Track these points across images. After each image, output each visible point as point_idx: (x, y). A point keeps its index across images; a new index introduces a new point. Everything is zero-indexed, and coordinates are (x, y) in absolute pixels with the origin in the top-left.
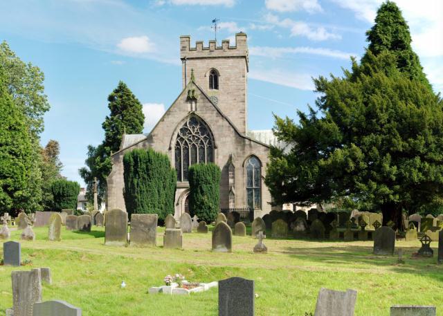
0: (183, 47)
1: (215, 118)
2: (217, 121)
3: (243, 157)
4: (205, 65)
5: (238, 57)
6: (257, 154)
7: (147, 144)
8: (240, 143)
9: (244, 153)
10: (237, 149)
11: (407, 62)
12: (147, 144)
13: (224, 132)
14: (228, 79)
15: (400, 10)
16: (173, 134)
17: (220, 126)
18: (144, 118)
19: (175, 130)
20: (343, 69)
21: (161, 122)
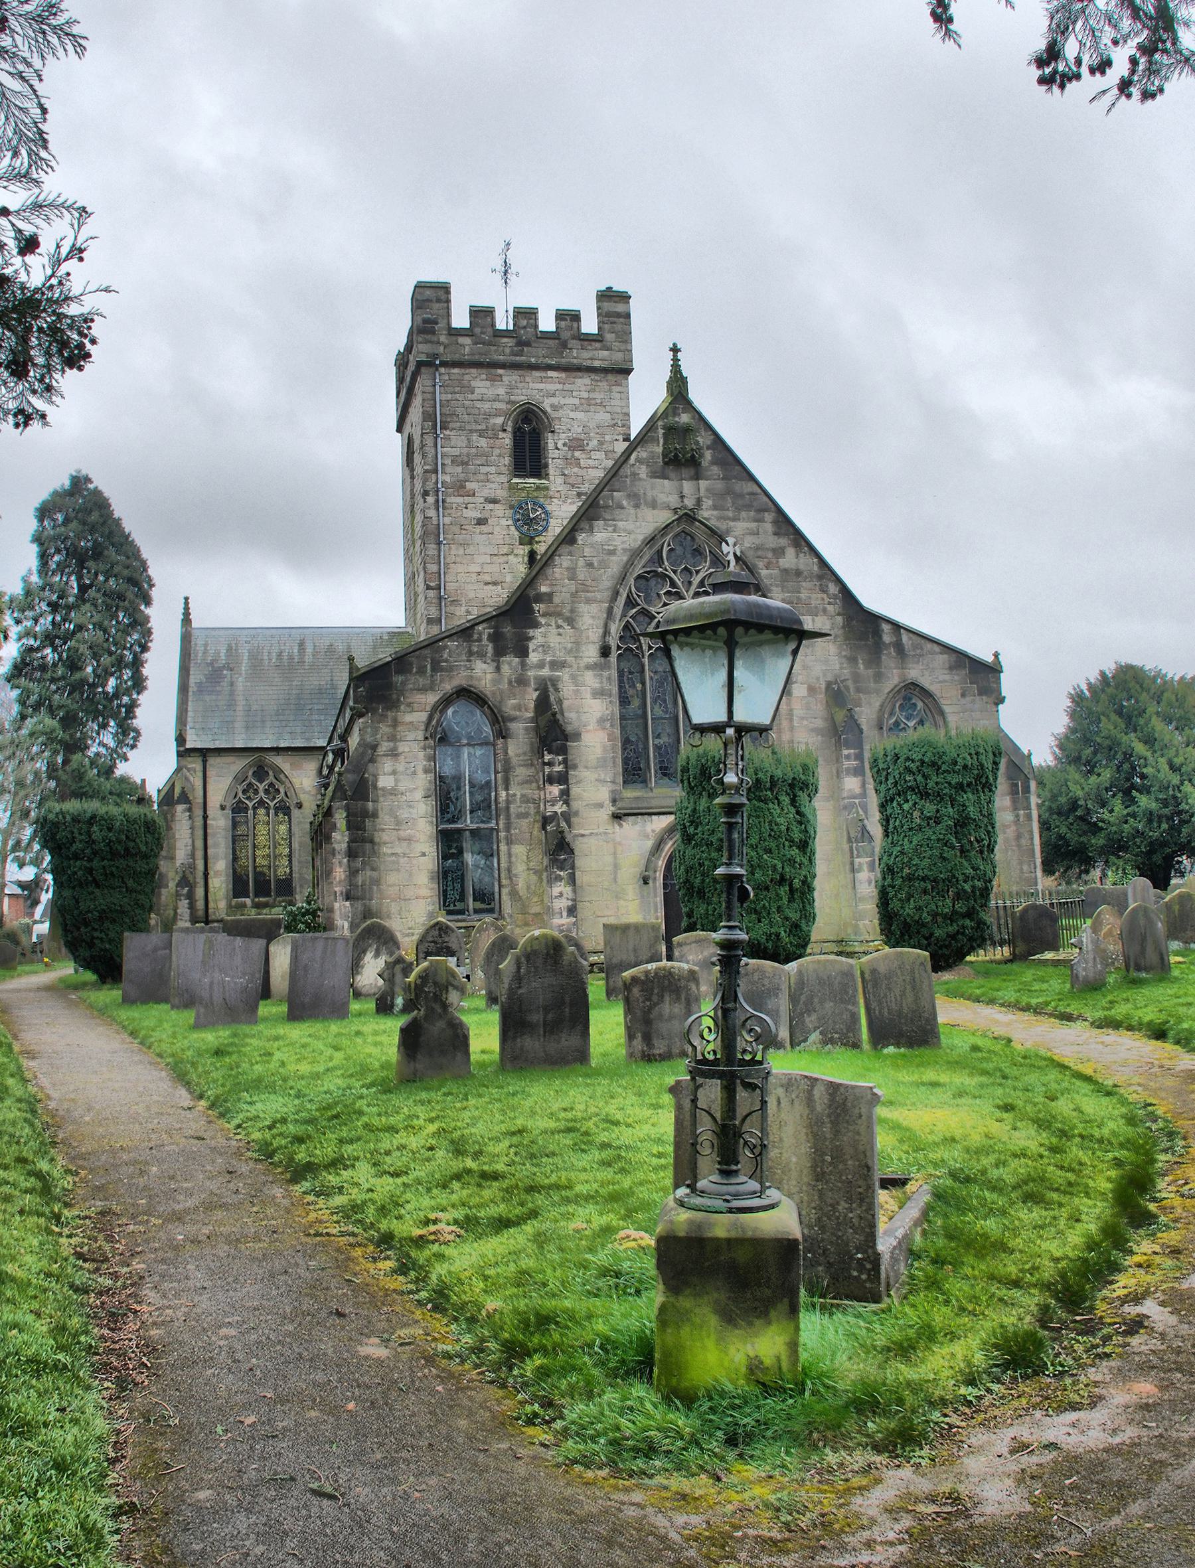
0: (425, 321)
1: (772, 541)
2: (779, 552)
3: (877, 692)
4: (501, 391)
5: (605, 371)
6: (925, 682)
7: (508, 630)
8: (863, 637)
9: (878, 677)
10: (852, 660)
11: (689, 405)
12: (508, 630)
13: (804, 595)
14: (577, 444)
15: (1109, 667)
16: (616, 594)
17: (786, 571)
18: (152, 586)
19: (623, 578)
20: (187, 619)
21: (565, 549)
